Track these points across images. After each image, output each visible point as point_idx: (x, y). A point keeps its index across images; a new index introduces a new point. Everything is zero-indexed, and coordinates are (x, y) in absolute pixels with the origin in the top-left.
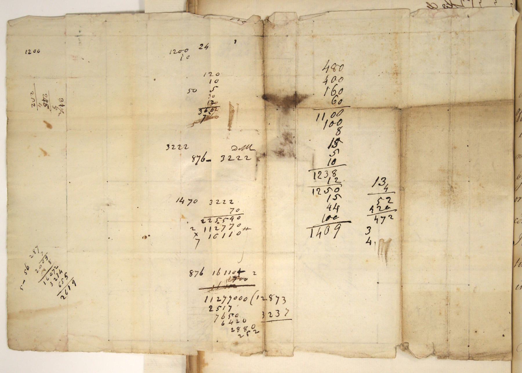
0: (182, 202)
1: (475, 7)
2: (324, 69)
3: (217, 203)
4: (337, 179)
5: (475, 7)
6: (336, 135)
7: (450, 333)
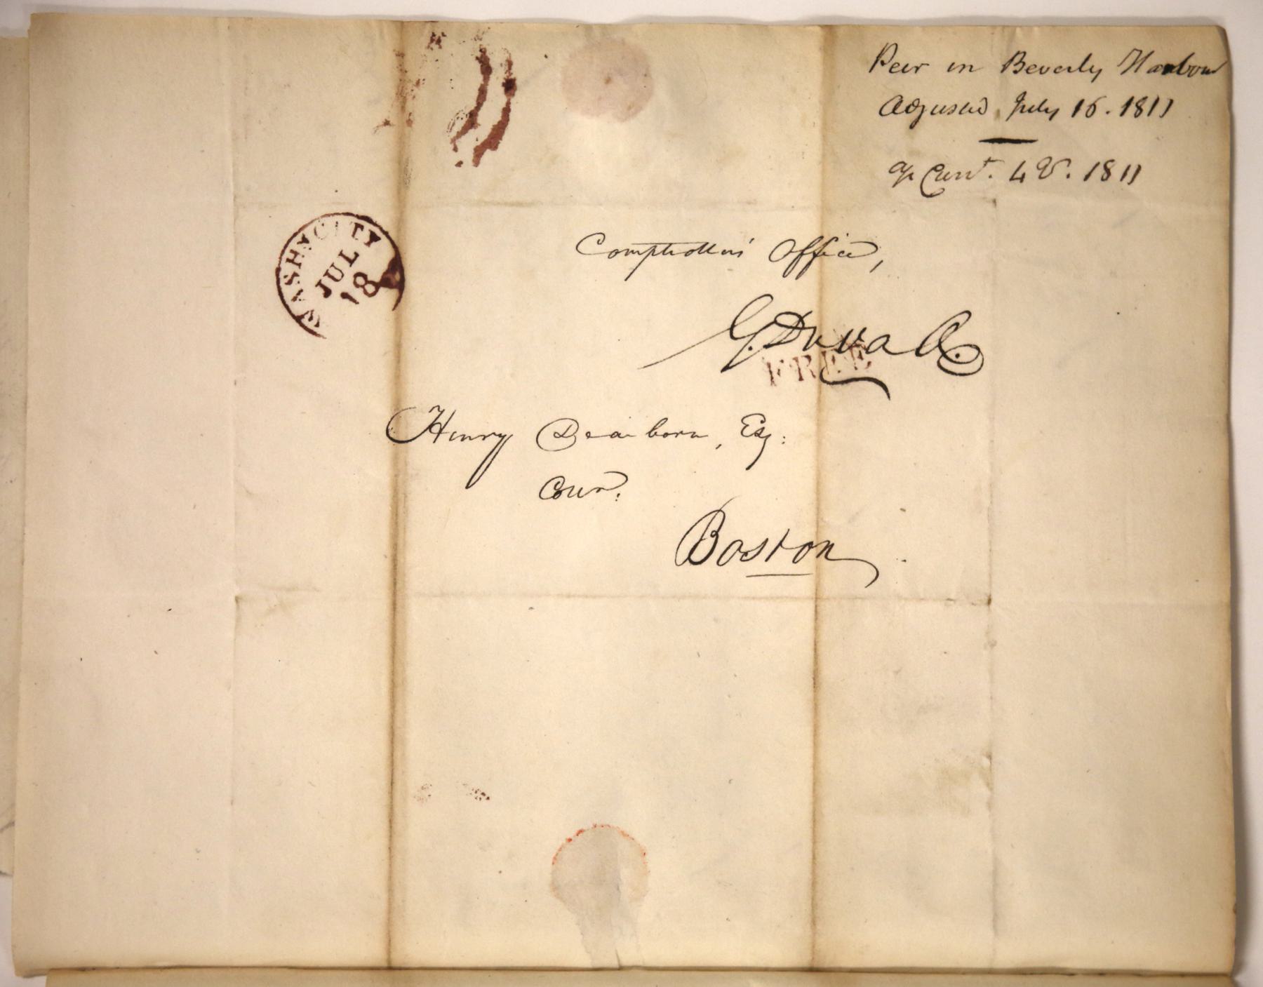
0: (1017, 179)
1: (929, 172)
2: (791, 254)
3: (1040, 178)
4: (364, 276)
5: (929, 172)
6: (1087, 116)
7: (1018, 177)
